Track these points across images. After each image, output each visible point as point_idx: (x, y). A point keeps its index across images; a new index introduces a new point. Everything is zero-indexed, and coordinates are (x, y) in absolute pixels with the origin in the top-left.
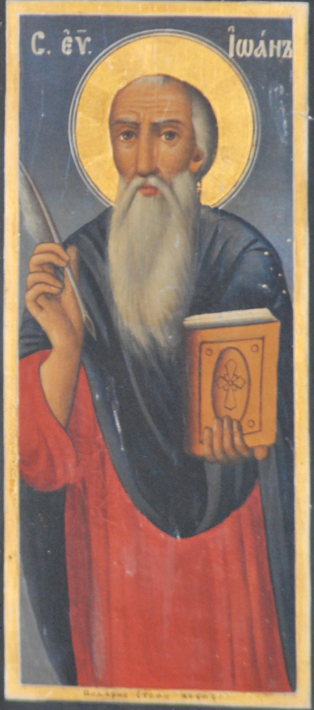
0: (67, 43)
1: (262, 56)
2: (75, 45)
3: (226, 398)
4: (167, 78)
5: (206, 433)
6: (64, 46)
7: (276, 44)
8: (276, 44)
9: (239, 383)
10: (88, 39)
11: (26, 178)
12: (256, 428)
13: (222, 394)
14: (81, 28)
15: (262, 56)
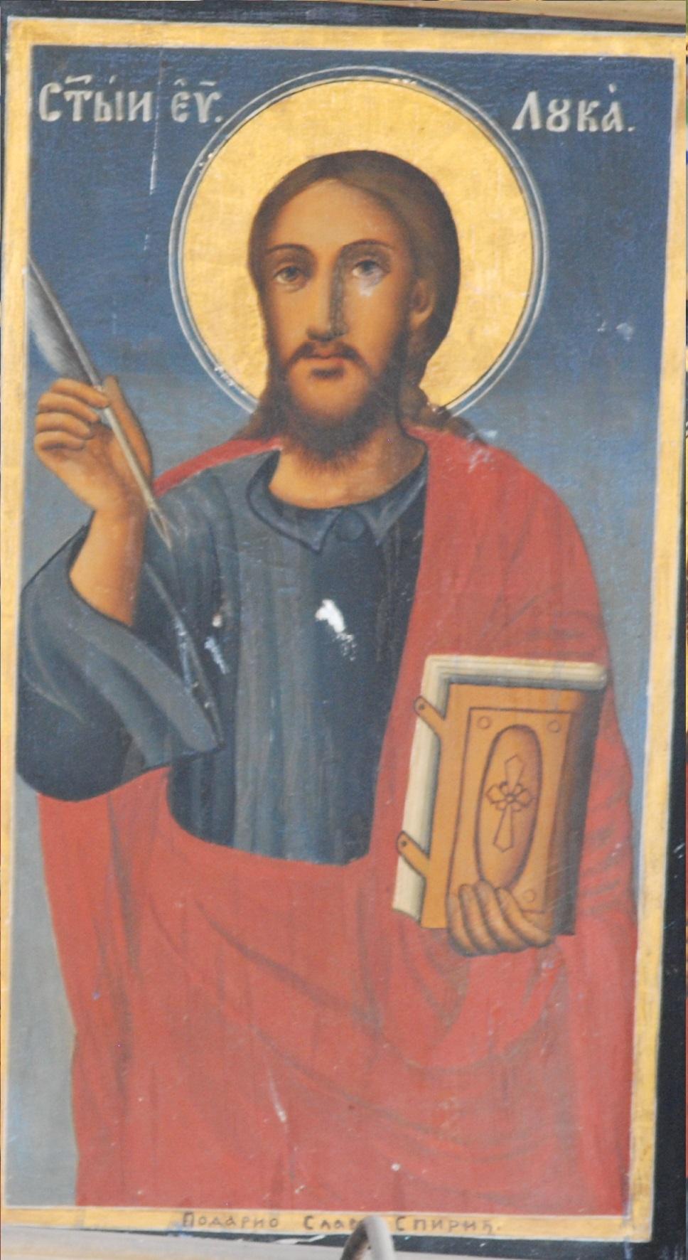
0: (180, 101)
1: (613, 129)
2: (192, 107)
3: (521, 774)
5: (504, 840)
6: (174, 107)
9: (496, 794)
10: (216, 96)
11: (40, 287)
12: (476, 714)
13: (528, 781)
14: (207, 79)
15: (613, 129)
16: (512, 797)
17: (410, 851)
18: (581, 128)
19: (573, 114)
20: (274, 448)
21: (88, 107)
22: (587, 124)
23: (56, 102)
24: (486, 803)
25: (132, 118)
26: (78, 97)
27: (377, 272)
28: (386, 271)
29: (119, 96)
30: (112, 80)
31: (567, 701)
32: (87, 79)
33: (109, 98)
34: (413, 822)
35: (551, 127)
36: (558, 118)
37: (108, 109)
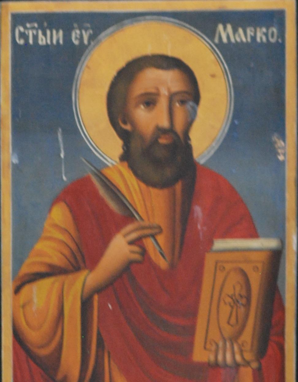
7: (225, 28)
9: (228, 300)
16: (236, 302)
20: (189, 107)
21: (35, 37)
22: (261, 39)
23: (23, 35)
24: (222, 304)
25: (55, 42)
26: (31, 33)
29: (48, 32)
31: (263, 257)
33: (45, 34)
36: (242, 36)
37: (44, 38)
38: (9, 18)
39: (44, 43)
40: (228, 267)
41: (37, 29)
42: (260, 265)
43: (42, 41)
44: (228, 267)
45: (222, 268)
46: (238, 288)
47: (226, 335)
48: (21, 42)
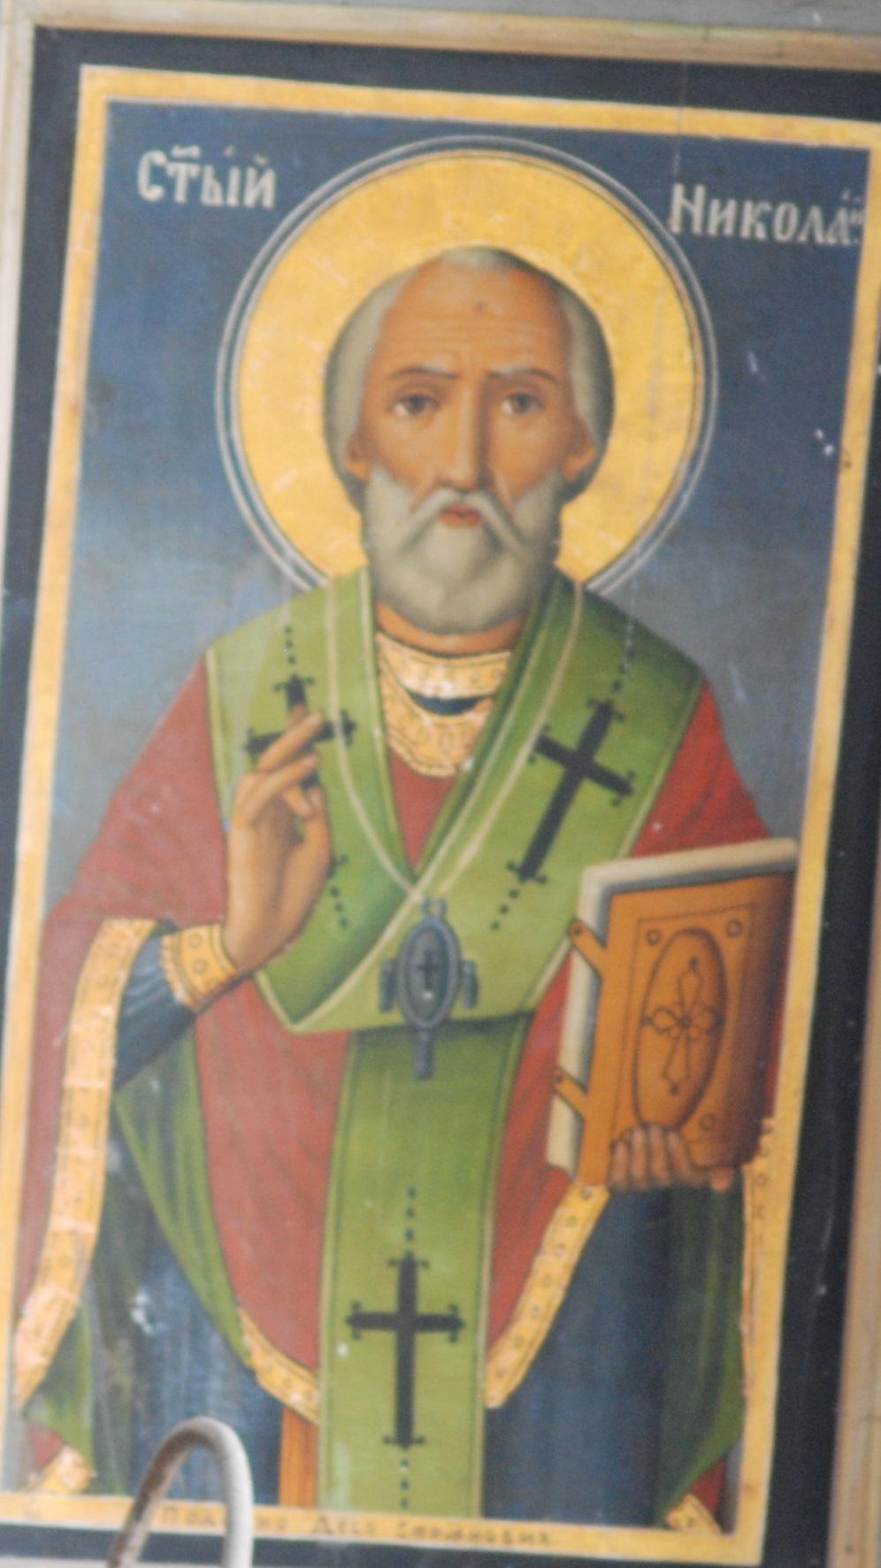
4: (550, 288)
7: (689, 195)
8: (689, 195)
16: (684, 1023)
17: (567, 1088)
18: (745, 233)
19: (767, 220)
21: (195, 187)
22: (753, 229)
23: (158, 175)
25: (712, 230)
26: (182, 173)
27: (533, 408)
28: (541, 405)
29: (234, 175)
30: (229, 151)
32: (194, 151)
33: (222, 178)
34: (570, 1059)
35: (780, 237)
38: (498, 1527)
39: (217, 200)
40: (668, 929)
41: (202, 161)
42: (742, 916)
43: (212, 195)
44: (668, 929)
45: (654, 938)
46: (691, 982)
47: (649, 1113)
48: (153, 193)
